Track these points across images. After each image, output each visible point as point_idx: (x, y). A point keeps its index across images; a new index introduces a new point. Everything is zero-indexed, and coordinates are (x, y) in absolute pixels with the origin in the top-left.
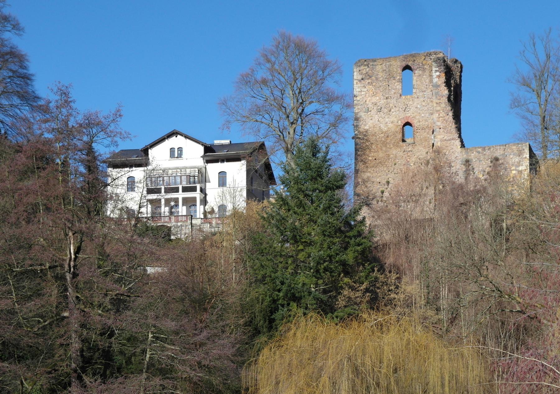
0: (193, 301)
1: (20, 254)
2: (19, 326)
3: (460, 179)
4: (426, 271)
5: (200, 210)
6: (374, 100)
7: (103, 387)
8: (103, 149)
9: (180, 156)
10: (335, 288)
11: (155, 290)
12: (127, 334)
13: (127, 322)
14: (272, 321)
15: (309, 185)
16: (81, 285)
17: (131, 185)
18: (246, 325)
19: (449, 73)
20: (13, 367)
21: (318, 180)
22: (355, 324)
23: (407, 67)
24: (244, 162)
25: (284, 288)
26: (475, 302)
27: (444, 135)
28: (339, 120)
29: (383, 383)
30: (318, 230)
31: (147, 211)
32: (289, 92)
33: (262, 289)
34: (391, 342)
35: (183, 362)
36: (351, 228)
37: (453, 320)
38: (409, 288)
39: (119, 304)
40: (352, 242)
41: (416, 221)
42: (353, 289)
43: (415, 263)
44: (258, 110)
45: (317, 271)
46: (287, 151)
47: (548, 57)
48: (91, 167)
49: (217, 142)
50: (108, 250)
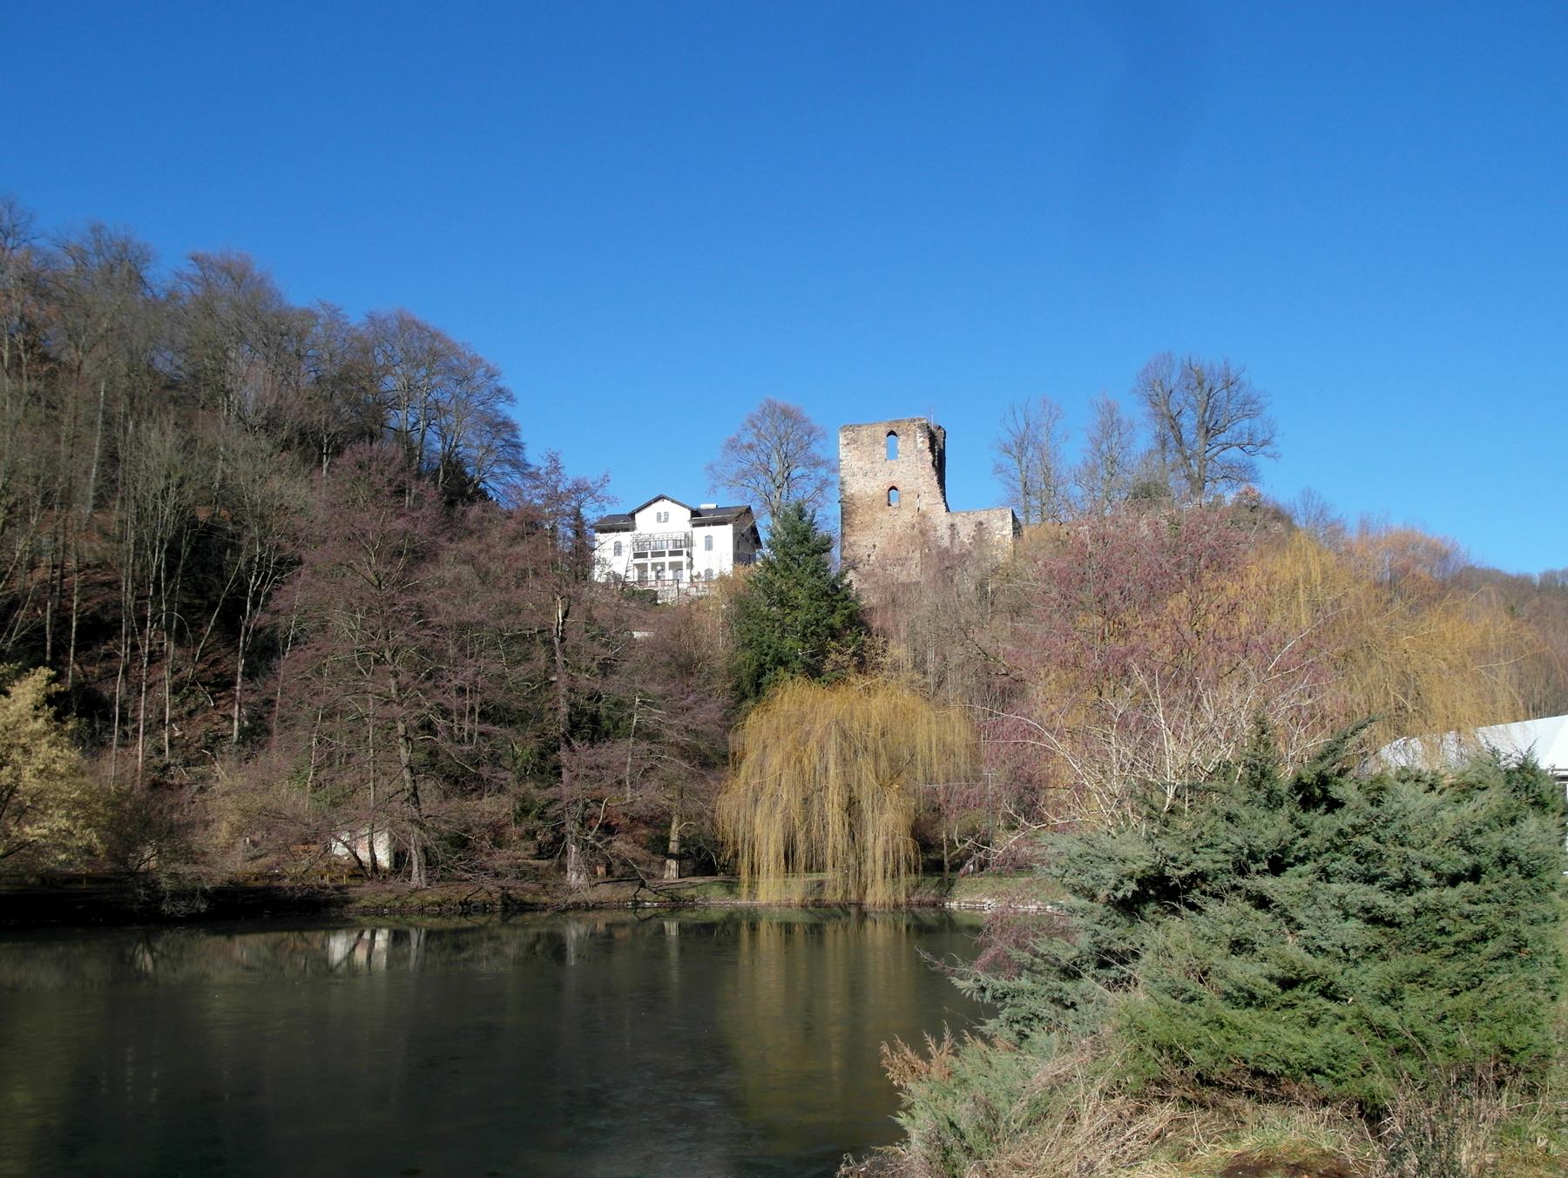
0: (679, 666)
1: (511, 618)
2: (510, 690)
3: (946, 543)
4: (913, 634)
5: (686, 574)
6: (860, 464)
7: (591, 751)
8: (591, 514)
9: (666, 520)
10: (822, 652)
11: (641, 655)
12: (613, 699)
13: (614, 686)
14: (759, 685)
15: (795, 548)
16: (569, 650)
17: (618, 549)
18: (733, 689)
19: (932, 439)
20: (503, 731)
21: (804, 544)
22: (843, 688)
23: (892, 433)
24: (730, 526)
25: (771, 652)
26: (961, 666)
27: (929, 499)
28: (824, 484)
29: (871, 746)
30: (805, 593)
31: (633, 576)
32: (775, 456)
33: (749, 653)
34: (878, 705)
35: (671, 727)
36: (838, 591)
37: (939, 685)
38: (896, 652)
39: (606, 668)
40: (839, 605)
41: (903, 584)
42: (840, 653)
43: (902, 627)
44: (744, 474)
45: (804, 635)
46: (773, 514)
47: (1028, 425)
48: (579, 533)
49: (703, 506)
50: (595, 613)
